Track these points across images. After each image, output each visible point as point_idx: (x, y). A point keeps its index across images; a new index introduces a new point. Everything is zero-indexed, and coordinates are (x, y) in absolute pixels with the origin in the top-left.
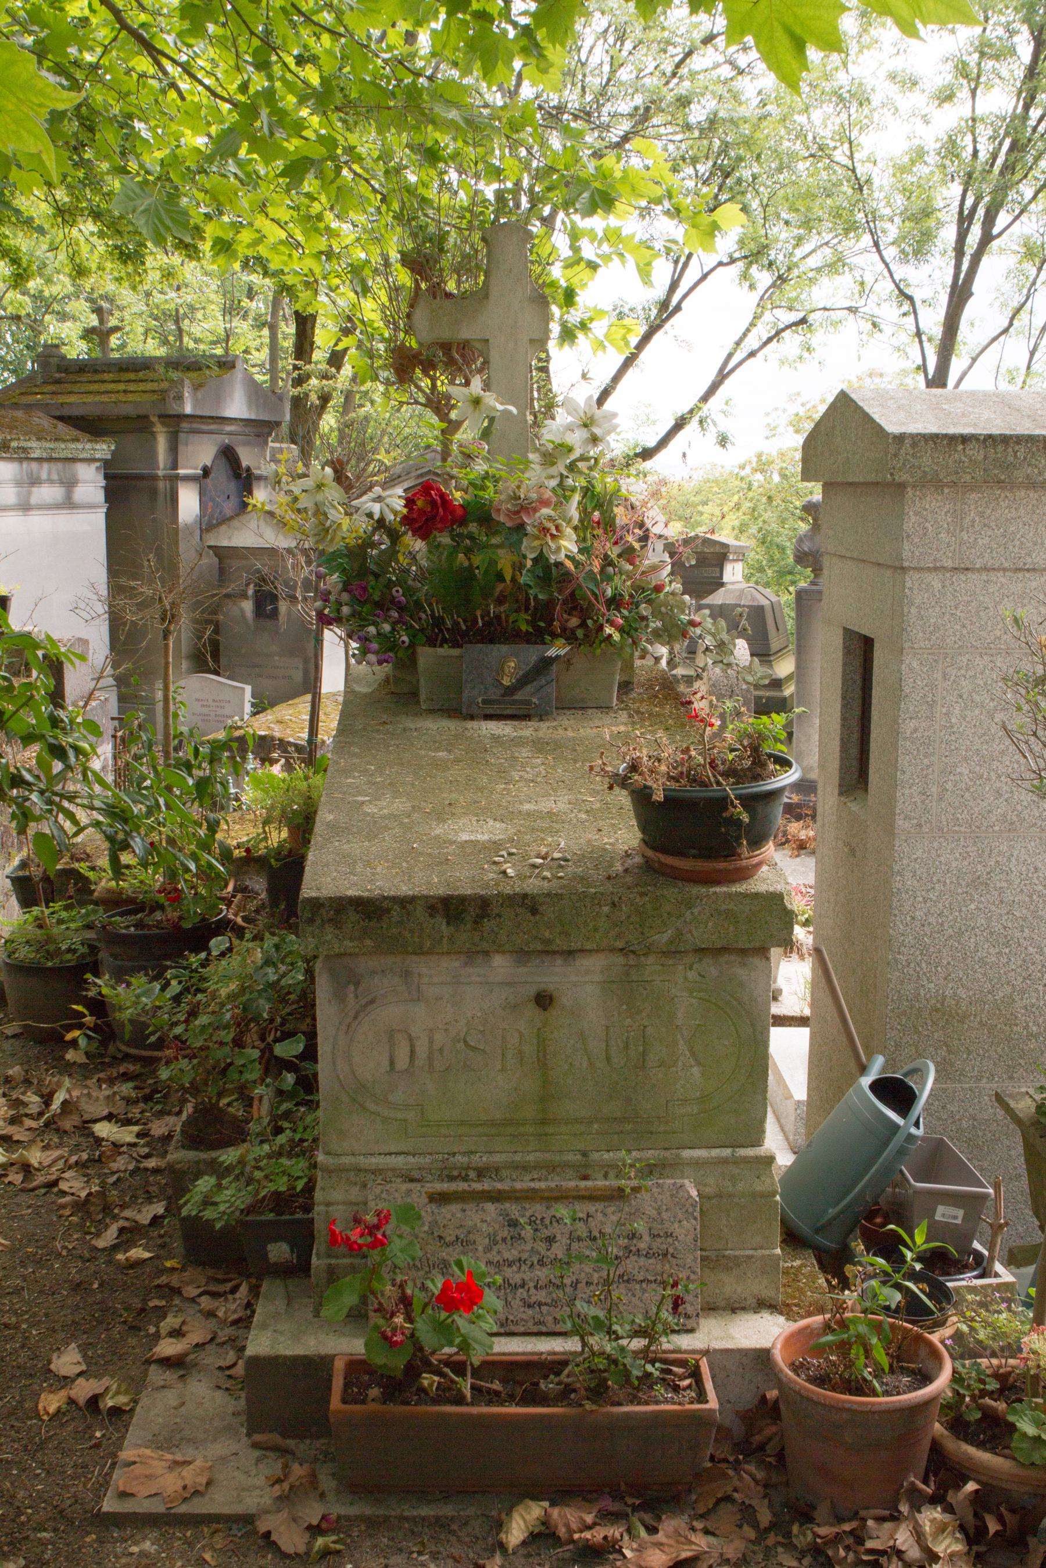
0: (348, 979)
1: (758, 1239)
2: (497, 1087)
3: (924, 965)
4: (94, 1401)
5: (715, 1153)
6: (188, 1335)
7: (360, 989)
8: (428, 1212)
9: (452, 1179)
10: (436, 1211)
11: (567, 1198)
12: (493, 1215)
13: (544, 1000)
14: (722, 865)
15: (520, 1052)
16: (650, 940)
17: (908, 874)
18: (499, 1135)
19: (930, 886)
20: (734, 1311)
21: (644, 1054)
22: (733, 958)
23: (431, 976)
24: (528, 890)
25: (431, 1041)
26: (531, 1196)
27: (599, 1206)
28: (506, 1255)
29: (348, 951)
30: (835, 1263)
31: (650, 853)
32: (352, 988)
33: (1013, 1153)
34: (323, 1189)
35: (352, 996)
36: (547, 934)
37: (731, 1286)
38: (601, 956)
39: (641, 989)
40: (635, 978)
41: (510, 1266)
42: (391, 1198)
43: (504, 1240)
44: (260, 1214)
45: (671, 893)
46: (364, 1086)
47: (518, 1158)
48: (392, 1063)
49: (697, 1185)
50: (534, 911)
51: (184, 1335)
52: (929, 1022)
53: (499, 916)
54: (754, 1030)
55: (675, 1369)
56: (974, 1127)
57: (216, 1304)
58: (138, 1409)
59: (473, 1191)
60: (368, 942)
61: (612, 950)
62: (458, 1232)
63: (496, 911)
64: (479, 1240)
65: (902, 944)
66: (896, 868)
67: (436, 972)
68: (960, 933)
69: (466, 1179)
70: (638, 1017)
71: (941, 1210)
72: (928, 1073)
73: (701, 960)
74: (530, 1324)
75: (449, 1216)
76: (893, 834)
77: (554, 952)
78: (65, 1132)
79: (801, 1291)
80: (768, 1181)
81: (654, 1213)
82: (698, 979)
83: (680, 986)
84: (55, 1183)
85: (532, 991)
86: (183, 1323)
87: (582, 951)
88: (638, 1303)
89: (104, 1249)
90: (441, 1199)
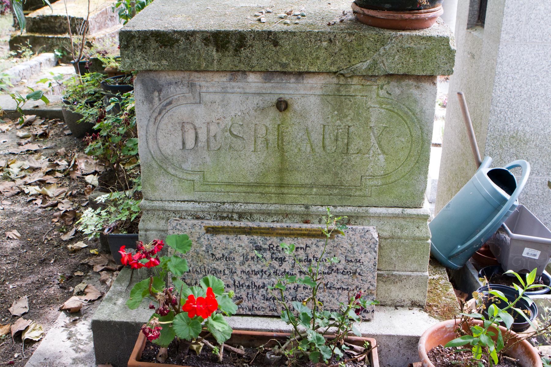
0: (153, 89)
1: (415, 266)
2: (251, 161)
3: (509, 113)
4: (20, 333)
5: (391, 210)
6: (88, 295)
7: (162, 94)
8: (206, 239)
9: (223, 218)
10: (210, 238)
11: (293, 234)
12: (247, 243)
13: (282, 106)
14: (407, 16)
15: (267, 140)
16: (355, 67)
17: (505, 64)
18: (253, 193)
19: (516, 71)
20: (396, 307)
21: (348, 144)
22: (411, 82)
23: (208, 87)
24: (272, 29)
25: (208, 131)
26: (270, 232)
27: (314, 240)
28: (254, 268)
29: (151, 68)
30: (463, 286)
31: (358, 9)
32: (156, 94)
33: (544, 212)
34: (143, 221)
35: (157, 99)
36: (284, 60)
37: (395, 292)
38: (321, 77)
39: (348, 102)
40: (343, 93)
41: (256, 274)
42: (182, 229)
43: (253, 258)
44: (120, 231)
45: (371, 34)
46: (166, 158)
47: (264, 207)
48: (184, 144)
49: (378, 229)
50: (276, 44)
51: (86, 294)
52: (509, 143)
53: (251, 46)
54: (422, 132)
55: (355, 346)
56: (526, 198)
57: (108, 277)
58: (43, 340)
59: (234, 228)
60: (164, 62)
61: (329, 73)
62: (224, 252)
63: (249, 43)
64: (237, 258)
65: (498, 102)
66: (499, 60)
67: (211, 84)
68: (530, 97)
69: (231, 219)
70: (345, 120)
71: (526, 250)
72: (526, 168)
73: (388, 83)
74: (267, 310)
75: (218, 242)
76: (499, 42)
77: (291, 73)
78: (73, 179)
79: (438, 295)
80: (424, 230)
81: (349, 247)
82: (387, 95)
83: (373, 99)
84: (56, 205)
85: (275, 99)
86: (87, 287)
87: (308, 73)
88: (336, 302)
89: (66, 241)
90: (213, 231)
